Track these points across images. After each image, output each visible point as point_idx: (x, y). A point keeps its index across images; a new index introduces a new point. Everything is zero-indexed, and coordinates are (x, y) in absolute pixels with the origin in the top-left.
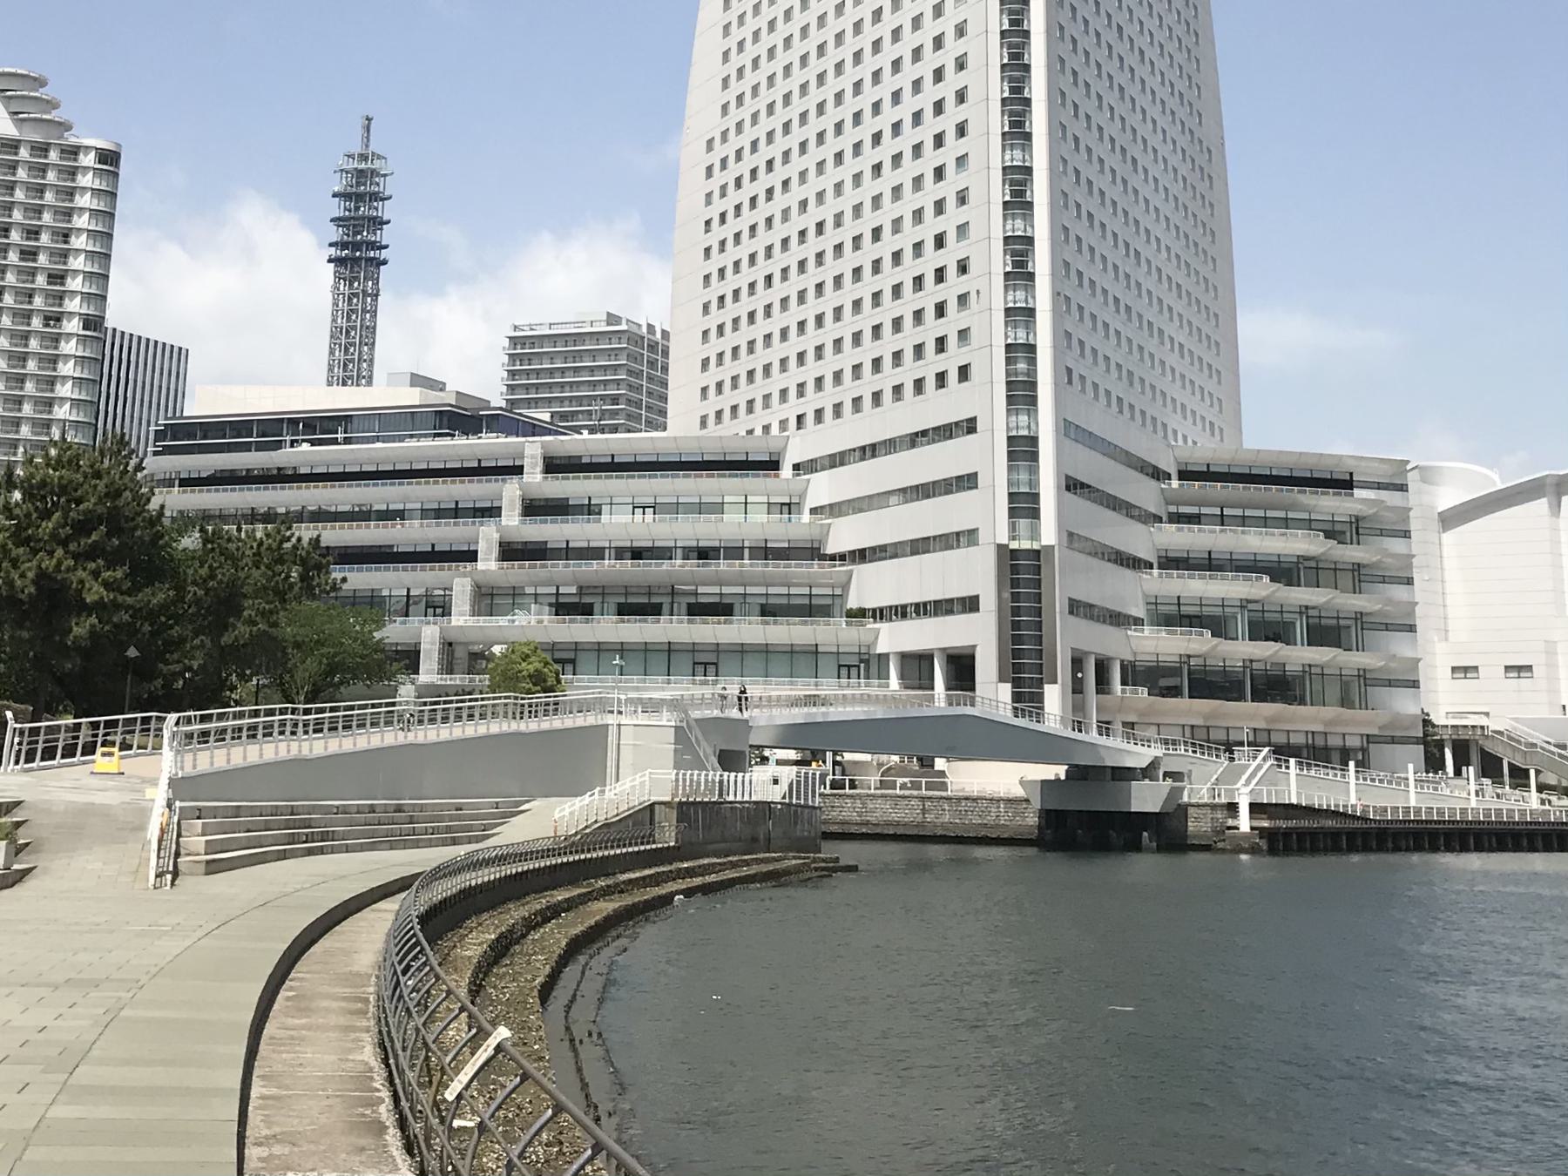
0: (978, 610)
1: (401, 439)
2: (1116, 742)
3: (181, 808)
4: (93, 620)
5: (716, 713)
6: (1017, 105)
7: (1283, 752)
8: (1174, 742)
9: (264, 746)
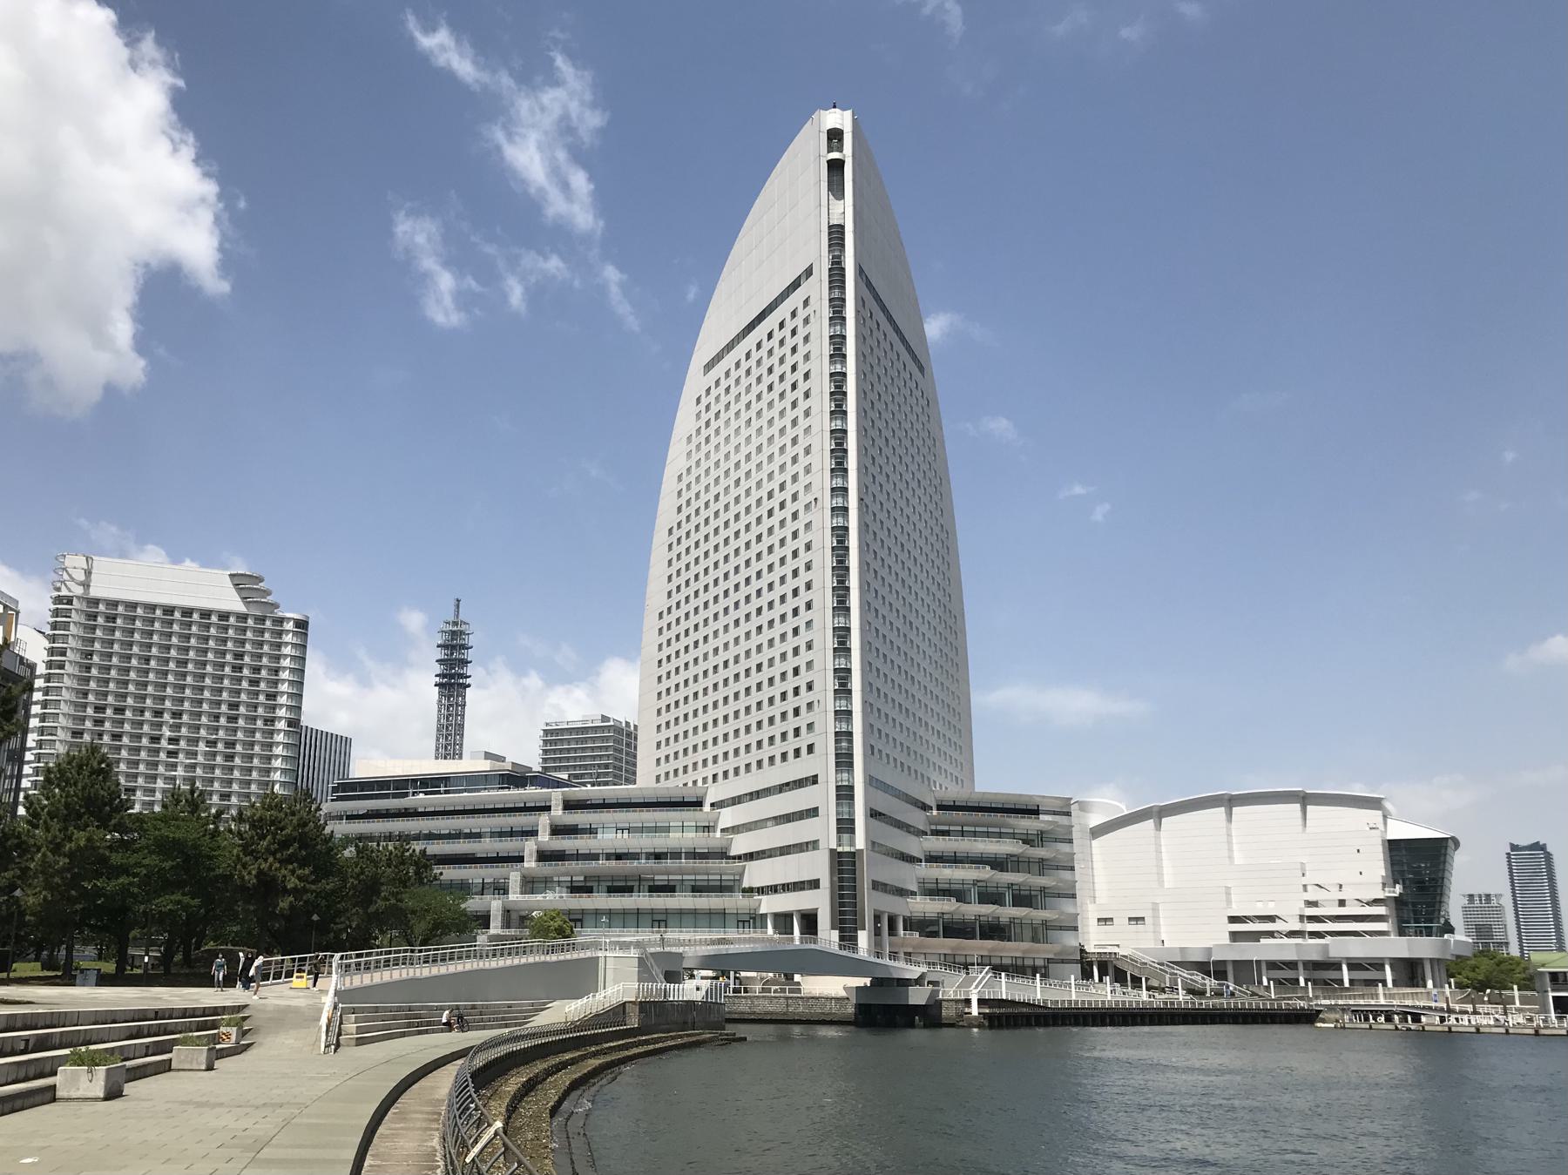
0: (819, 888)
1: (478, 790)
2: (901, 964)
3: (342, 1008)
4: (291, 898)
5: (659, 949)
6: (841, 591)
7: (997, 969)
8: (934, 964)
9: (384, 973)
